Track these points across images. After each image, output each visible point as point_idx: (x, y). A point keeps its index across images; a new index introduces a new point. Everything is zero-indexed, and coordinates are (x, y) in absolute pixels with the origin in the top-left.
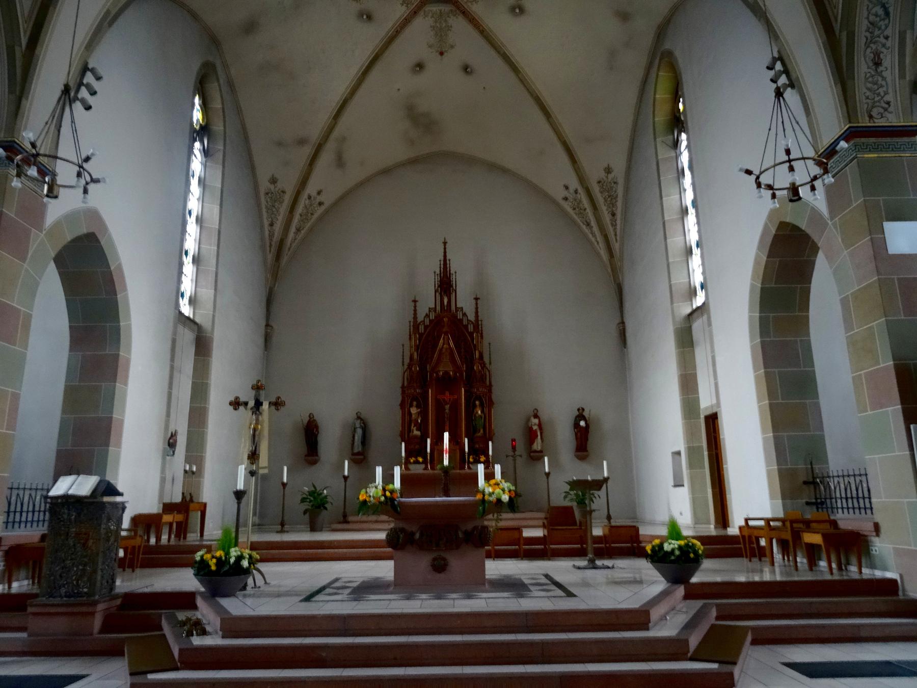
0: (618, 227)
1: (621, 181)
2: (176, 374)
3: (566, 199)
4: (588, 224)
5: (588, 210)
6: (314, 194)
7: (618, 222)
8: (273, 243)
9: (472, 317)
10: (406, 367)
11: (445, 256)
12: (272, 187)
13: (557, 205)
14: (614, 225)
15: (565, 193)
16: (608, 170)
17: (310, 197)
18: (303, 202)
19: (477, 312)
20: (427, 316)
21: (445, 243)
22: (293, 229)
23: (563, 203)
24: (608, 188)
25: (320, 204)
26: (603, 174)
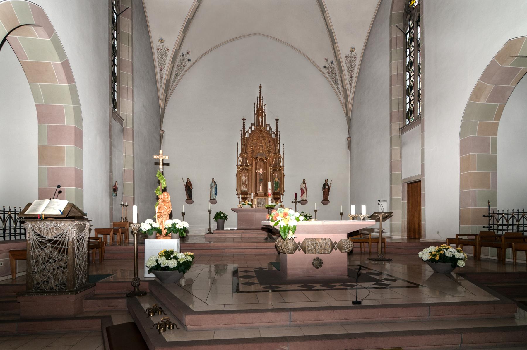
0: (353, 84)
1: (359, 57)
2: (114, 149)
3: (325, 67)
4: (336, 83)
5: (337, 74)
6: (185, 53)
7: (353, 82)
8: (163, 82)
9: (274, 130)
10: (239, 155)
11: (260, 95)
12: (161, 45)
13: (321, 71)
14: (351, 83)
15: (325, 64)
16: (352, 50)
17: (183, 55)
18: (179, 58)
19: (277, 127)
20: (250, 128)
21: (260, 87)
22: (174, 75)
23: (324, 70)
24: (350, 60)
25: (189, 60)
26: (348, 52)
